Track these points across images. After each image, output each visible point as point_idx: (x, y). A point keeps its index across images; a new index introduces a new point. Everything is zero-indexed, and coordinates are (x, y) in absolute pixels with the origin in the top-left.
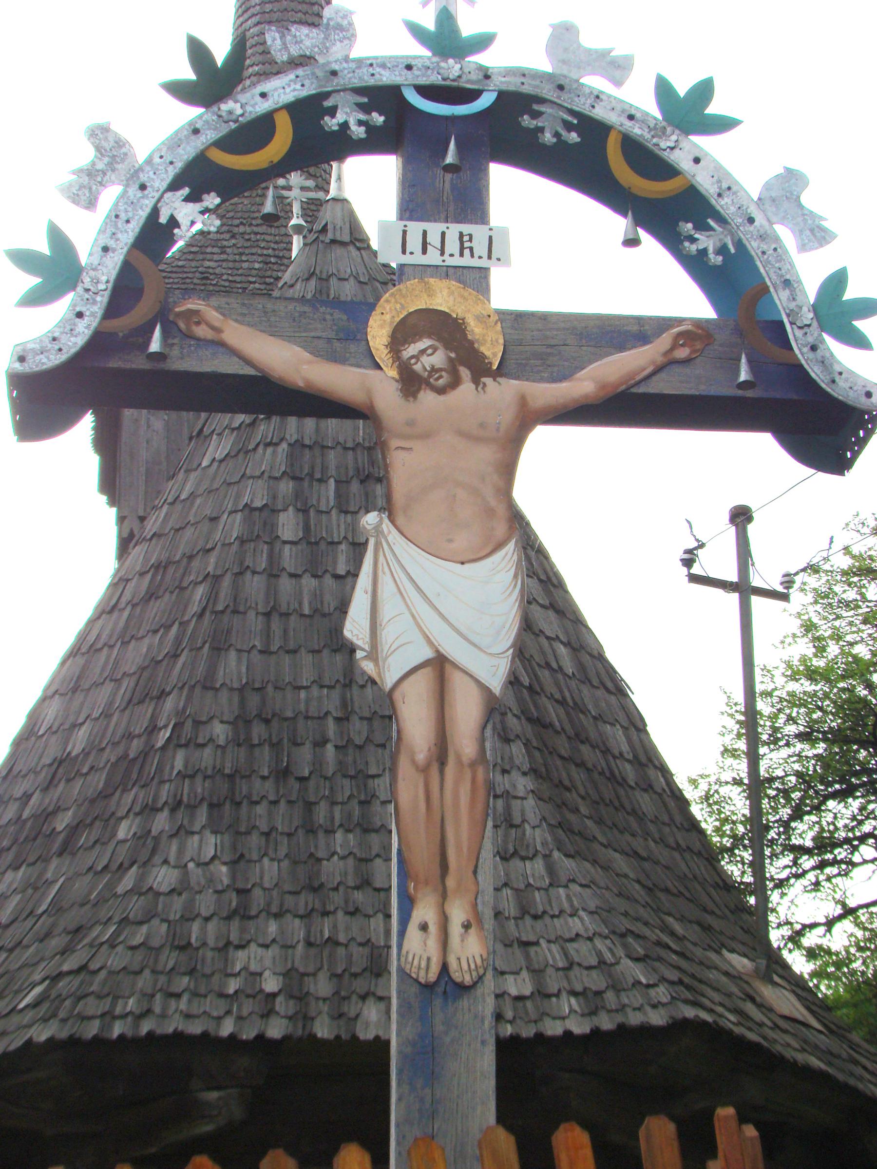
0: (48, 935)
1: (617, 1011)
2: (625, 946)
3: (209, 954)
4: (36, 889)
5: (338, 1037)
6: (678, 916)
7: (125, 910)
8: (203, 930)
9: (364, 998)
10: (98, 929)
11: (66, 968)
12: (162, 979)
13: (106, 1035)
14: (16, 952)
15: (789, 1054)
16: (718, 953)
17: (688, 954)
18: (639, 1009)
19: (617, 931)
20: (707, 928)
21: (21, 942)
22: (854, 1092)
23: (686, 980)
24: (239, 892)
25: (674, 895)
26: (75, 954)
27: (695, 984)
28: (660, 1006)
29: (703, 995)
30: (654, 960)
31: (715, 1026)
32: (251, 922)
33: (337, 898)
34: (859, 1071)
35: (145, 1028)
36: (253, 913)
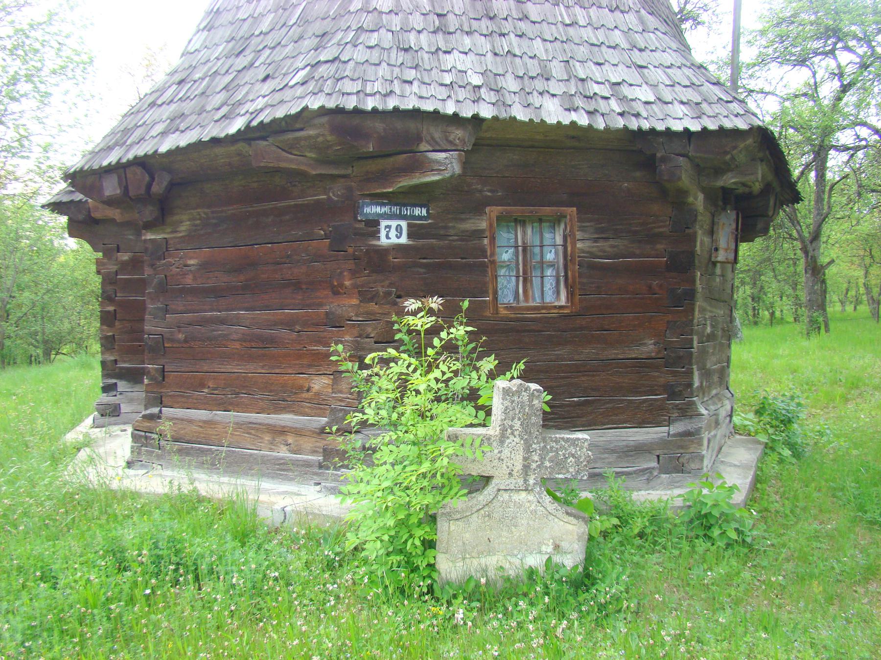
0: (301, 38)
3: (426, 56)
4: (285, 10)
7: (359, 22)
10: (340, 35)
11: (322, 58)
12: (397, 70)
13: (361, 106)
14: (277, 49)
21: (280, 43)
24: (439, 15)
26: (326, 51)
33: (507, 27)
35: (391, 104)
36: (451, 30)
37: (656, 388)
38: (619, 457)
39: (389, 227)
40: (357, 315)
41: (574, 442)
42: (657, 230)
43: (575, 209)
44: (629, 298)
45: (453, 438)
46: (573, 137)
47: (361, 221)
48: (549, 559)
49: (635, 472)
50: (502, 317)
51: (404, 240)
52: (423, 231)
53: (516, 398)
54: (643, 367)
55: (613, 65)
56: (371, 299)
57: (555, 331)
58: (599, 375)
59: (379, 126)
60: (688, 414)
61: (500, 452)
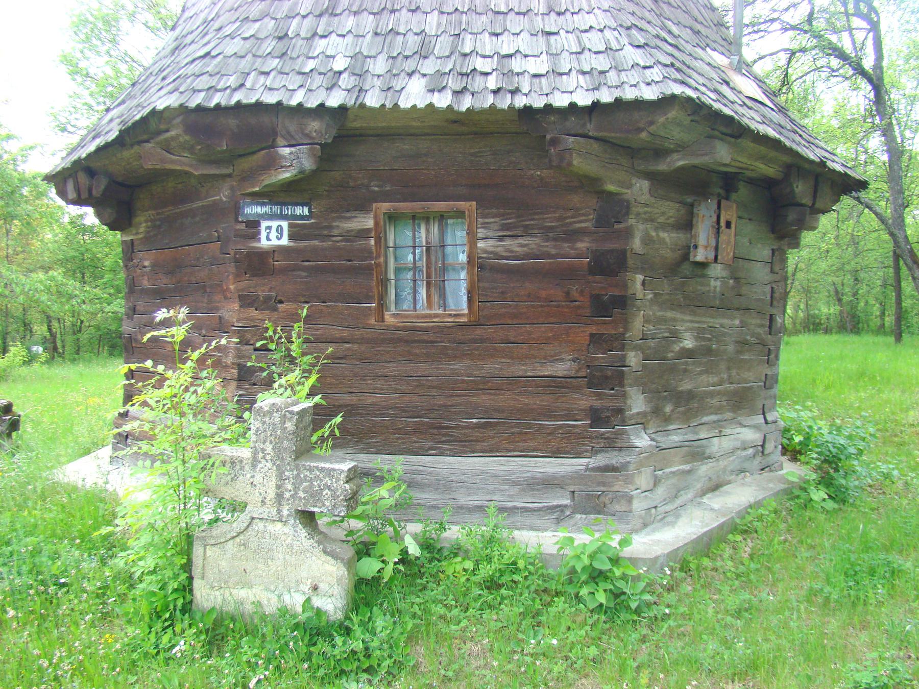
1: (617, 87)
2: (629, 36)
5: (383, 106)
6: (676, 21)
8: (300, 26)
9: (410, 75)
15: (753, 126)
16: (703, 49)
17: (682, 48)
18: (635, 86)
19: (625, 25)
20: (698, 33)
22: (797, 155)
23: (677, 64)
25: (674, 7)
27: (684, 68)
28: (653, 84)
29: (690, 77)
30: (652, 48)
31: (697, 101)
32: (336, 18)
34: (797, 138)
37: (575, 412)
38: (523, 489)
39: (269, 228)
40: (238, 321)
41: (329, 473)
42: (578, 225)
43: (474, 203)
44: (542, 306)
45: (863, 439)
46: (455, 122)
47: (242, 222)
48: (308, 600)
49: (539, 509)
50: (388, 326)
51: (285, 241)
52: (305, 231)
53: (267, 419)
54: (558, 387)
55: (513, 34)
56: (250, 305)
57: (449, 342)
58: (503, 394)
59: (232, 122)
60: (616, 445)
61: (253, 477)
